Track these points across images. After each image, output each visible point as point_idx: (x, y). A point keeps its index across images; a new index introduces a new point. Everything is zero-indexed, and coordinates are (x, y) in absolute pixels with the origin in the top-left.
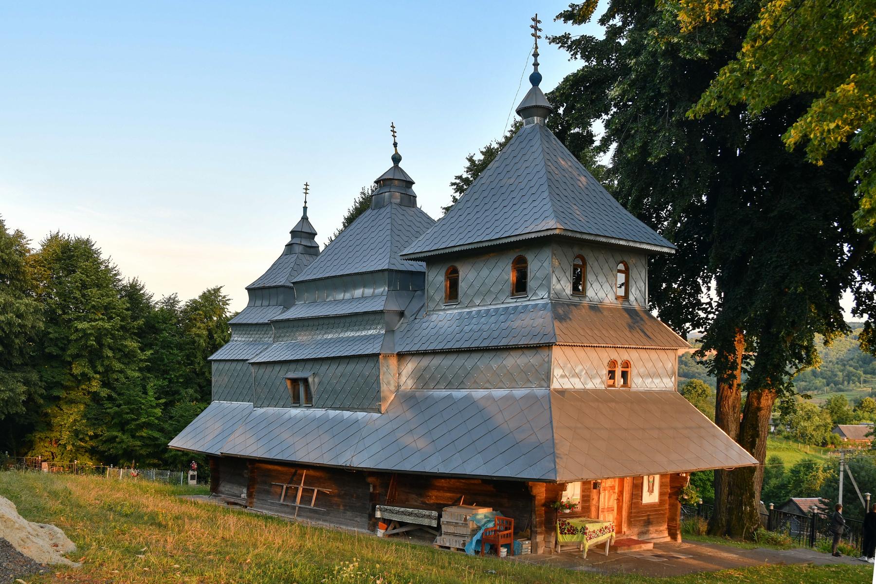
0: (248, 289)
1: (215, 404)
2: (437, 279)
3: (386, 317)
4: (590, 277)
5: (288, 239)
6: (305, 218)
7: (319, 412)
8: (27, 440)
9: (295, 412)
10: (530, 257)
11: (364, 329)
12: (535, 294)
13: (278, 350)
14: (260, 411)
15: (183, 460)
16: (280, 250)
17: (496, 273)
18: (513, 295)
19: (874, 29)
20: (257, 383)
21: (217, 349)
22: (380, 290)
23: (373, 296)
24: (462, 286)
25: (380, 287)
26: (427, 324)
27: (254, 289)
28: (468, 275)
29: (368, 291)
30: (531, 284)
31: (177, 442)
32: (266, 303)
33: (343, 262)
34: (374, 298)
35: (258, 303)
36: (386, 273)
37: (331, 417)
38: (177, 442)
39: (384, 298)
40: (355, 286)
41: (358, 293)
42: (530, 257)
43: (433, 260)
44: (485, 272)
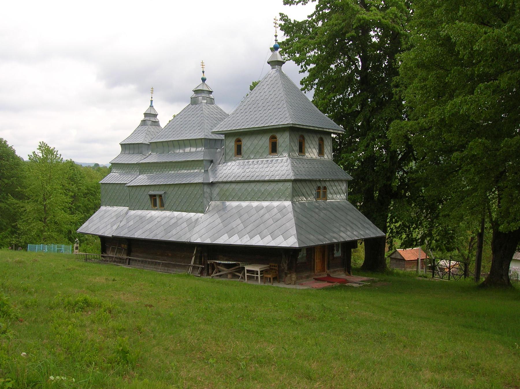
0: (121, 145)
1: (103, 208)
2: (231, 144)
3: (204, 163)
4: (307, 145)
5: (142, 117)
6: (151, 106)
7: (168, 213)
8: (395, 189)
9: (154, 213)
10: (278, 136)
11: (192, 169)
12: (281, 154)
13: (142, 179)
14: (132, 212)
15: (84, 238)
16: (139, 123)
17: (261, 143)
18: (270, 154)
19: (426, 386)
20: (129, 197)
21: (105, 177)
22: (199, 149)
23: (196, 152)
24: (244, 149)
25: (200, 147)
26: (226, 167)
27: (125, 144)
28: (247, 143)
29: (193, 150)
30: (279, 149)
31: (82, 229)
32: (131, 152)
33: (178, 132)
34: (198, 153)
35: (127, 152)
36: (203, 141)
37: (176, 215)
38: (82, 229)
39: (203, 153)
40: (185, 146)
41: (187, 150)
42: (278, 136)
43: (228, 135)
44: (256, 142)
